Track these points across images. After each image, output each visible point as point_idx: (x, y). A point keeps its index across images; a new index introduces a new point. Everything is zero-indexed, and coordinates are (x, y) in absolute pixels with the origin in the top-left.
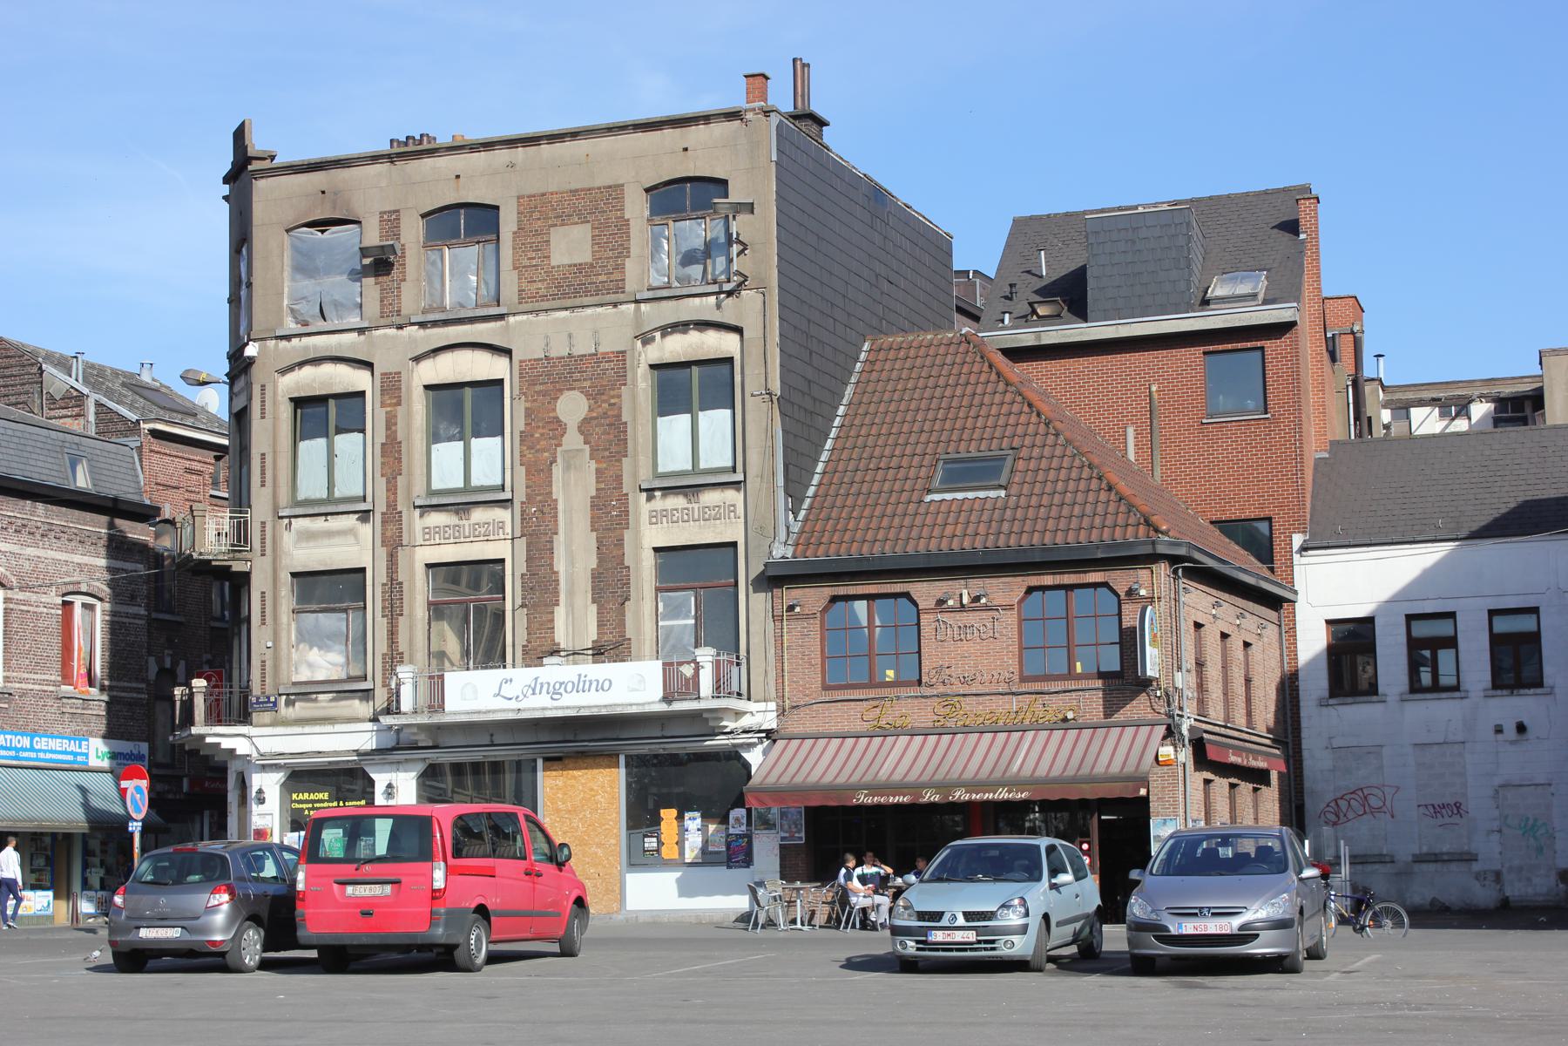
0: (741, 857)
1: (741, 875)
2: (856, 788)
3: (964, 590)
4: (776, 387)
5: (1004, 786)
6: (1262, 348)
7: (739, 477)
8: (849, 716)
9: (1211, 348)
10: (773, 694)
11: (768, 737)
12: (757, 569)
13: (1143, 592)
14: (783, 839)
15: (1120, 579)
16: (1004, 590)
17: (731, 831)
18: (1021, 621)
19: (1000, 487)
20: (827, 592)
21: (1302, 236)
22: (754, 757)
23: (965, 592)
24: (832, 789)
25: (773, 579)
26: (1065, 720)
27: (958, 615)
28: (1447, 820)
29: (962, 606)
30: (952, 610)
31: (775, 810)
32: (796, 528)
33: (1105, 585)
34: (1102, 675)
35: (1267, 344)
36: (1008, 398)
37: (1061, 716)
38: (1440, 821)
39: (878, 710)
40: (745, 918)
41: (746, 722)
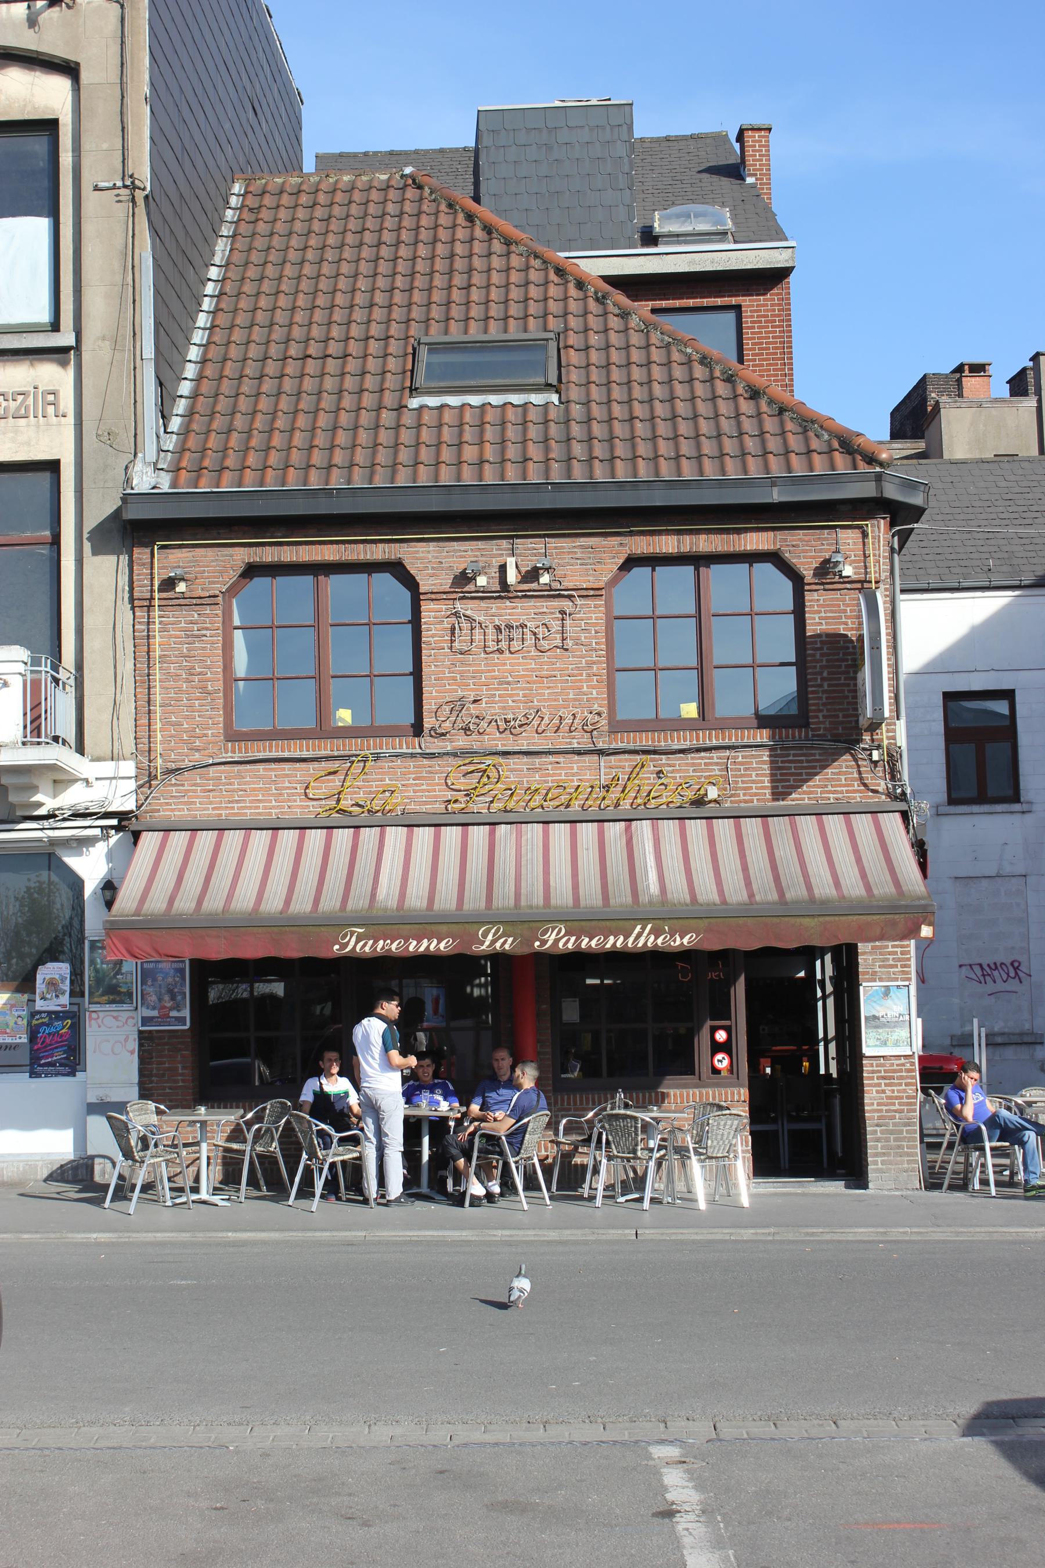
0: (59, 1056)
1: (57, 1088)
2: (340, 923)
3: (512, 557)
4: (144, 173)
5: (644, 921)
6: (738, 308)
7: (65, 338)
8: (281, 789)
9: (664, 304)
10: (129, 745)
11: (118, 829)
12: (102, 507)
13: (848, 571)
14: (145, 1021)
15: (804, 547)
16: (582, 560)
17: (40, 1005)
18: (612, 619)
19: (548, 387)
20: (241, 556)
21: (750, 180)
22: (91, 867)
23: (511, 562)
24: (285, 924)
25: (134, 530)
26: (699, 802)
27: (494, 606)
28: (1000, 986)
29: (504, 585)
30: (484, 595)
31: (129, 965)
32: (170, 443)
33: (774, 558)
34: (763, 721)
35: (745, 301)
36: (516, 261)
37: (690, 795)
38: (990, 987)
39: (336, 781)
40: (78, 1176)
41: (74, 797)
